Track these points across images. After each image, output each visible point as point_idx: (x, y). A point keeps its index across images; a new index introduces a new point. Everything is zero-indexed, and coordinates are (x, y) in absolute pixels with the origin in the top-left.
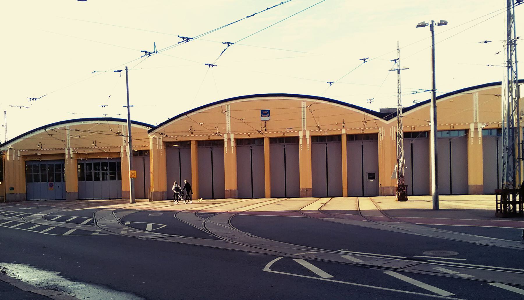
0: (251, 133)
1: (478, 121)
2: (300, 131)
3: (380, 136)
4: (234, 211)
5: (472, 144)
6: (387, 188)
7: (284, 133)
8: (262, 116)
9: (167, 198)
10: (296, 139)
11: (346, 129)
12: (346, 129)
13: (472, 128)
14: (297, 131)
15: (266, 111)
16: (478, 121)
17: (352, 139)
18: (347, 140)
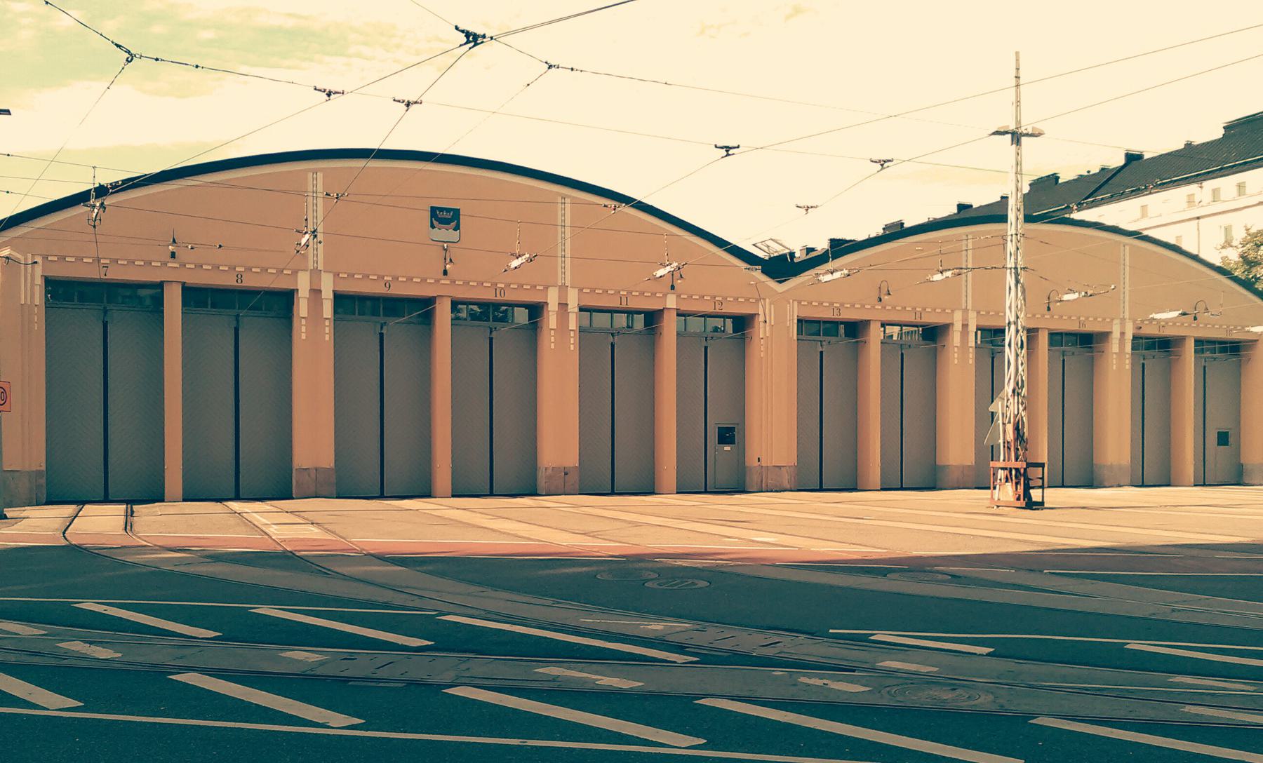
0: (842, 305)
1: (1127, 316)
2: (550, 289)
3: (762, 324)
4: (136, 561)
5: (304, 336)
6: (777, 469)
7: (502, 288)
8: (433, 226)
9: (580, 490)
10: (286, 298)
11: (678, 296)
12: (677, 296)
13: (552, 300)
14: (542, 288)
15: (448, 210)
16: (969, 307)
17: (201, 303)
18: (184, 304)
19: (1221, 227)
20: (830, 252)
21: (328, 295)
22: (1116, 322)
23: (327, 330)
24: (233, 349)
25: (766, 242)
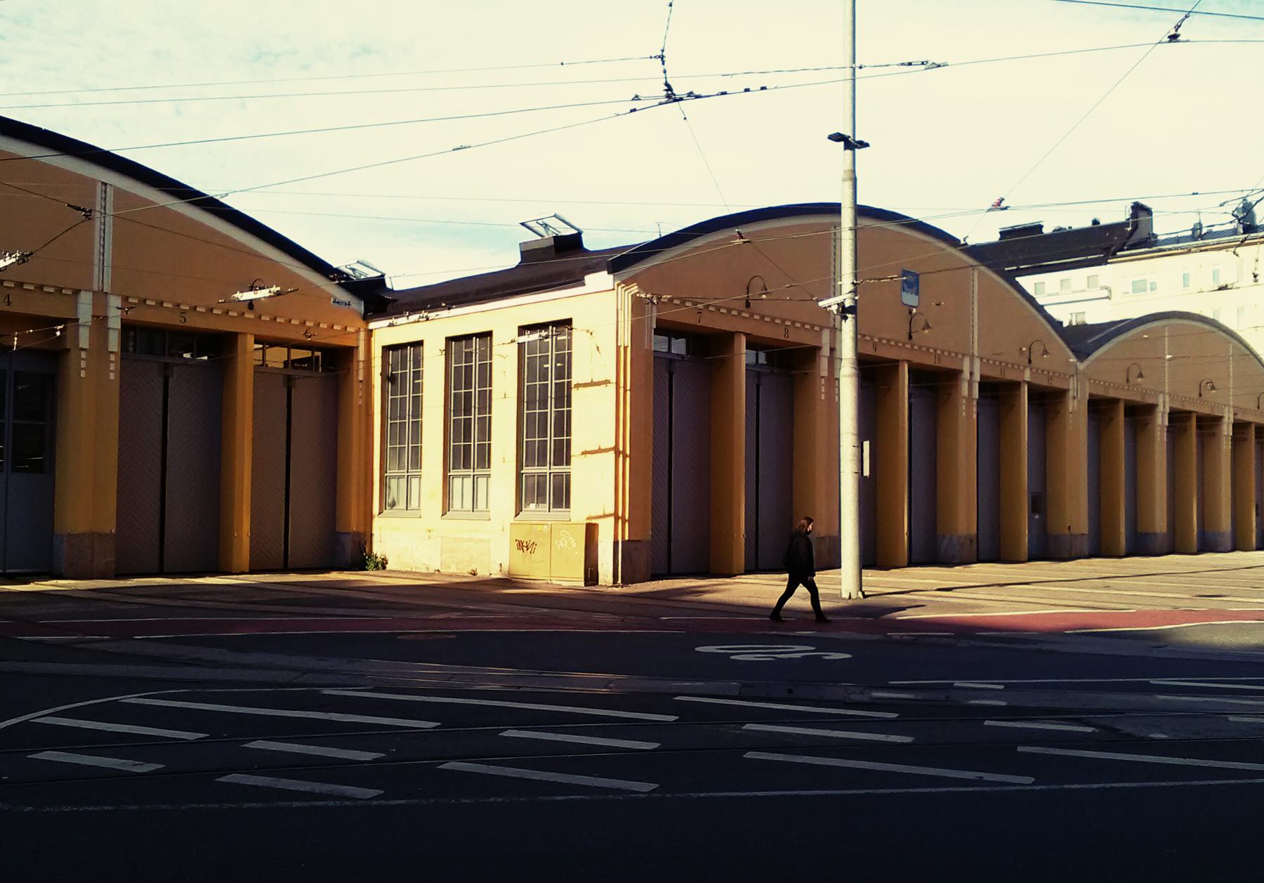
19: (999, 206)
20: (1040, 235)
21: (115, 323)
22: (86, 299)
23: (112, 367)
24: (160, 427)
25: (544, 220)
